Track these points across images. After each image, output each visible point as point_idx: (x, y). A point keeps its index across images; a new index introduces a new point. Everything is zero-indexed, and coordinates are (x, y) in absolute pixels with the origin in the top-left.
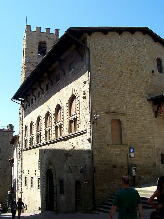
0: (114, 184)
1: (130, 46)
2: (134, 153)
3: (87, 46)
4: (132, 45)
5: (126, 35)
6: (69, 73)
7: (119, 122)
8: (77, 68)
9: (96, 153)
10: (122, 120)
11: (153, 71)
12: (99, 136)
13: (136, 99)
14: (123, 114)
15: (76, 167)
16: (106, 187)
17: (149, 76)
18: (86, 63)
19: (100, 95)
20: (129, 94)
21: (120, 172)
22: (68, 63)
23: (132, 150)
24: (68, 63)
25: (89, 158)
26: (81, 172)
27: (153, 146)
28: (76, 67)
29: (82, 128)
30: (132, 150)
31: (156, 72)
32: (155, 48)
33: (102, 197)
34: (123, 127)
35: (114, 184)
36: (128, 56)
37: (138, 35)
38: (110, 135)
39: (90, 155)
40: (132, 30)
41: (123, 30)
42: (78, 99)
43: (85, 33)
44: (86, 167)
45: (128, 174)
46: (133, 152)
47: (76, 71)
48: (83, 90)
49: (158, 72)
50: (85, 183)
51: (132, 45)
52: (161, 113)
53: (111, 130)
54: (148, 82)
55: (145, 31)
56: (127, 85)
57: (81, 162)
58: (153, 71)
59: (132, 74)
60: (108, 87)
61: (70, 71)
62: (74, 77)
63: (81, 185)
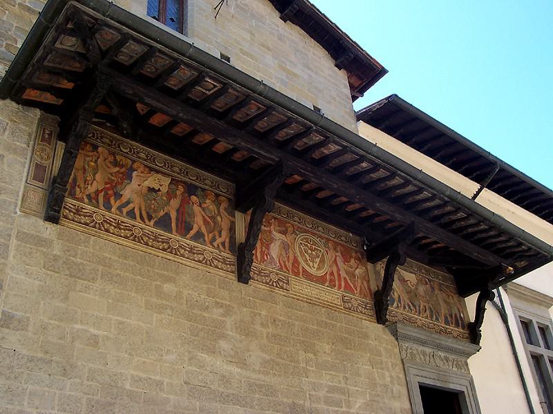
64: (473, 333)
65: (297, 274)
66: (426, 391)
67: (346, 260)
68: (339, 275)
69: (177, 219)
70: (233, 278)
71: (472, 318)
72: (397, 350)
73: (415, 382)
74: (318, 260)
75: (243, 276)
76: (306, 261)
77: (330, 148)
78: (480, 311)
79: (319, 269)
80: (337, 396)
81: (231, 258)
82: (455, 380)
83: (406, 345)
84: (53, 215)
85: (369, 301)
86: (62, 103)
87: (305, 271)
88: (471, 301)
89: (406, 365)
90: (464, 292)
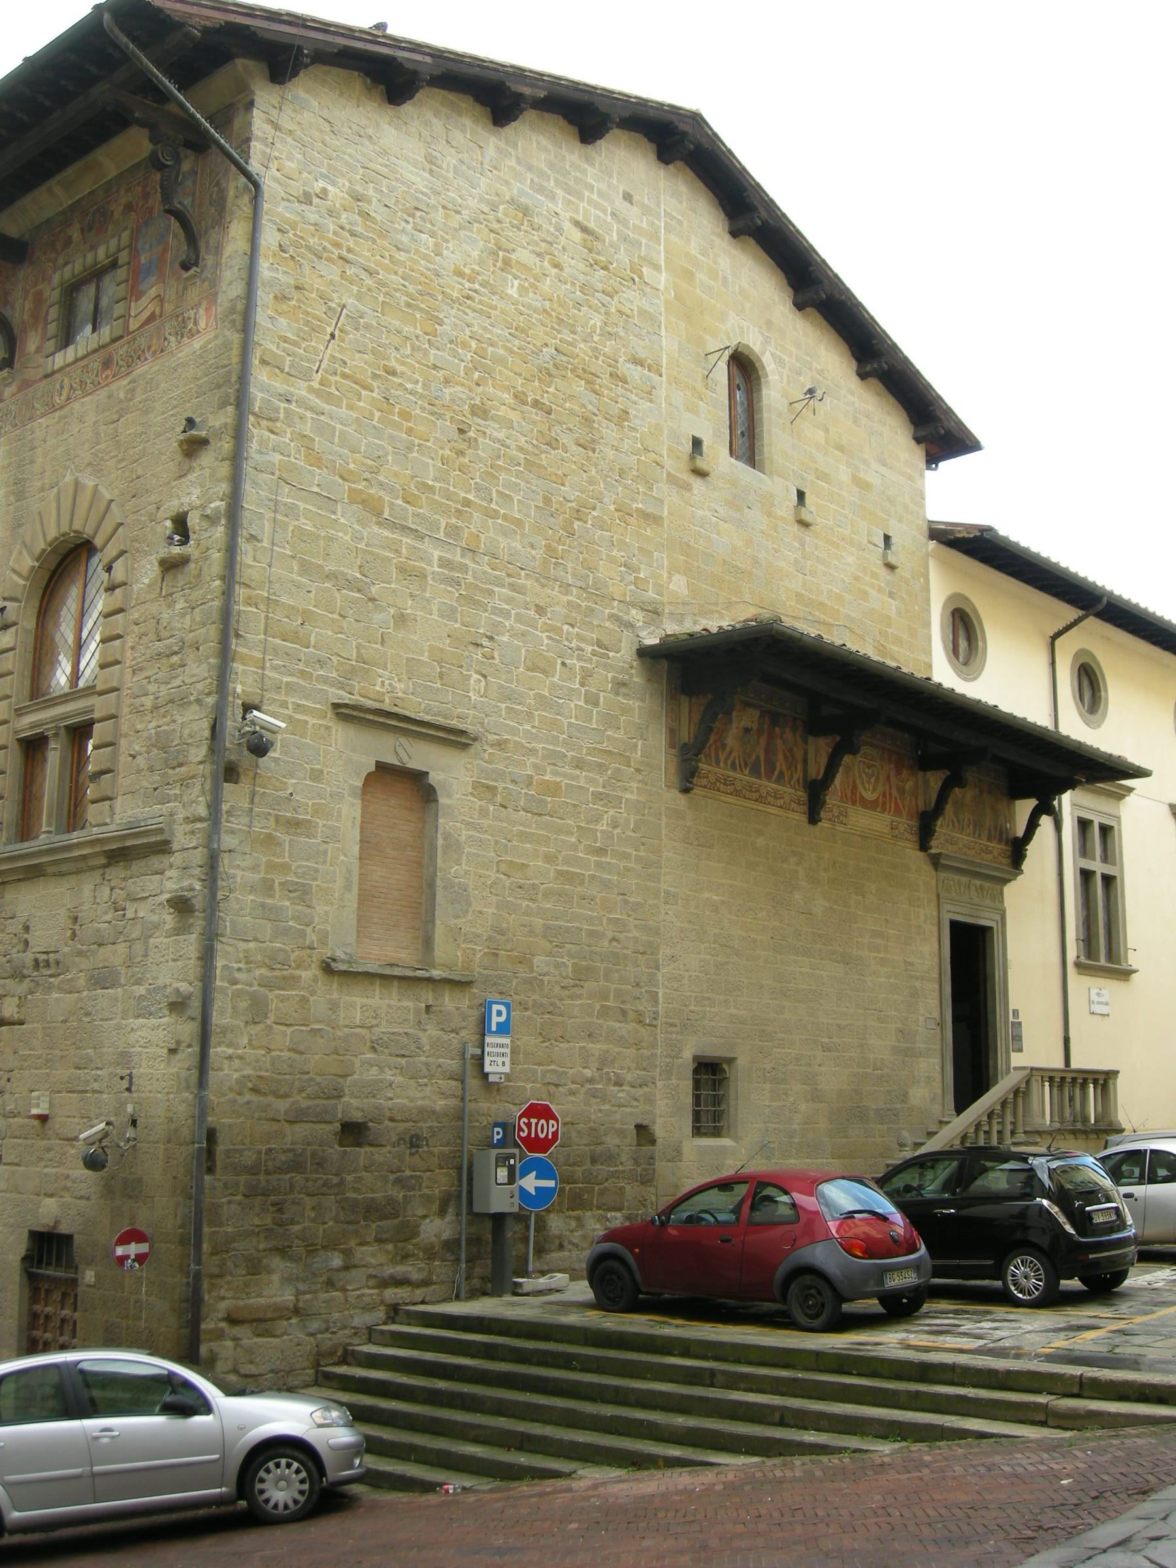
0: (347, 1268)
1: (559, 229)
2: (507, 1041)
3: (246, 154)
4: (577, 224)
5: (536, 146)
6: (59, 360)
7: (417, 787)
8: (134, 325)
9: (226, 1021)
10: (442, 776)
11: (697, 443)
12: (267, 887)
13: (558, 631)
14: (455, 738)
15: (43, 1119)
16: (287, 1297)
17: (669, 474)
18: (221, 298)
19: (306, 568)
20: (513, 587)
21: (398, 1181)
22: (56, 278)
23: (495, 1019)
24: (56, 278)
25: (172, 1051)
26: (93, 1163)
27: (644, 1006)
28: (125, 317)
29: (119, 812)
30: (499, 1013)
31: (718, 456)
32: (725, 279)
33: (253, 1369)
34: (447, 836)
35: (347, 1268)
36: (531, 299)
37: (624, 166)
38: (348, 888)
39: (188, 1030)
40: (586, 114)
41: (527, 91)
42: (119, 573)
43: (245, 57)
44: (134, 1123)
45: (459, 1197)
46: (503, 1029)
47: (121, 350)
48: (174, 506)
49: (731, 452)
50: (120, 1251)
51: (577, 224)
52: (722, 757)
53: (357, 848)
54: (656, 520)
55: (679, 141)
56: (505, 517)
57: (96, 1086)
58: (697, 443)
59: (553, 443)
60: (371, 508)
61: (67, 338)
62: (103, 393)
63: (72, 1266)
64: (1017, 851)
65: (854, 803)
66: (954, 925)
67: (899, 773)
68: (891, 794)
69: (765, 760)
70: (804, 818)
71: (1020, 832)
72: (934, 882)
73: (946, 918)
74: (873, 780)
75: (813, 819)
76: (863, 784)
77: (368, 189)
78: (1032, 825)
79: (874, 790)
80: (878, 941)
81: (802, 795)
82: (987, 915)
83: (943, 875)
84: (686, 790)
85: (915, 823)
86: (726, 1222)
87: (862, 797)
88: (1025, 807)
89: (942, 900)
90: (1017, 792)
